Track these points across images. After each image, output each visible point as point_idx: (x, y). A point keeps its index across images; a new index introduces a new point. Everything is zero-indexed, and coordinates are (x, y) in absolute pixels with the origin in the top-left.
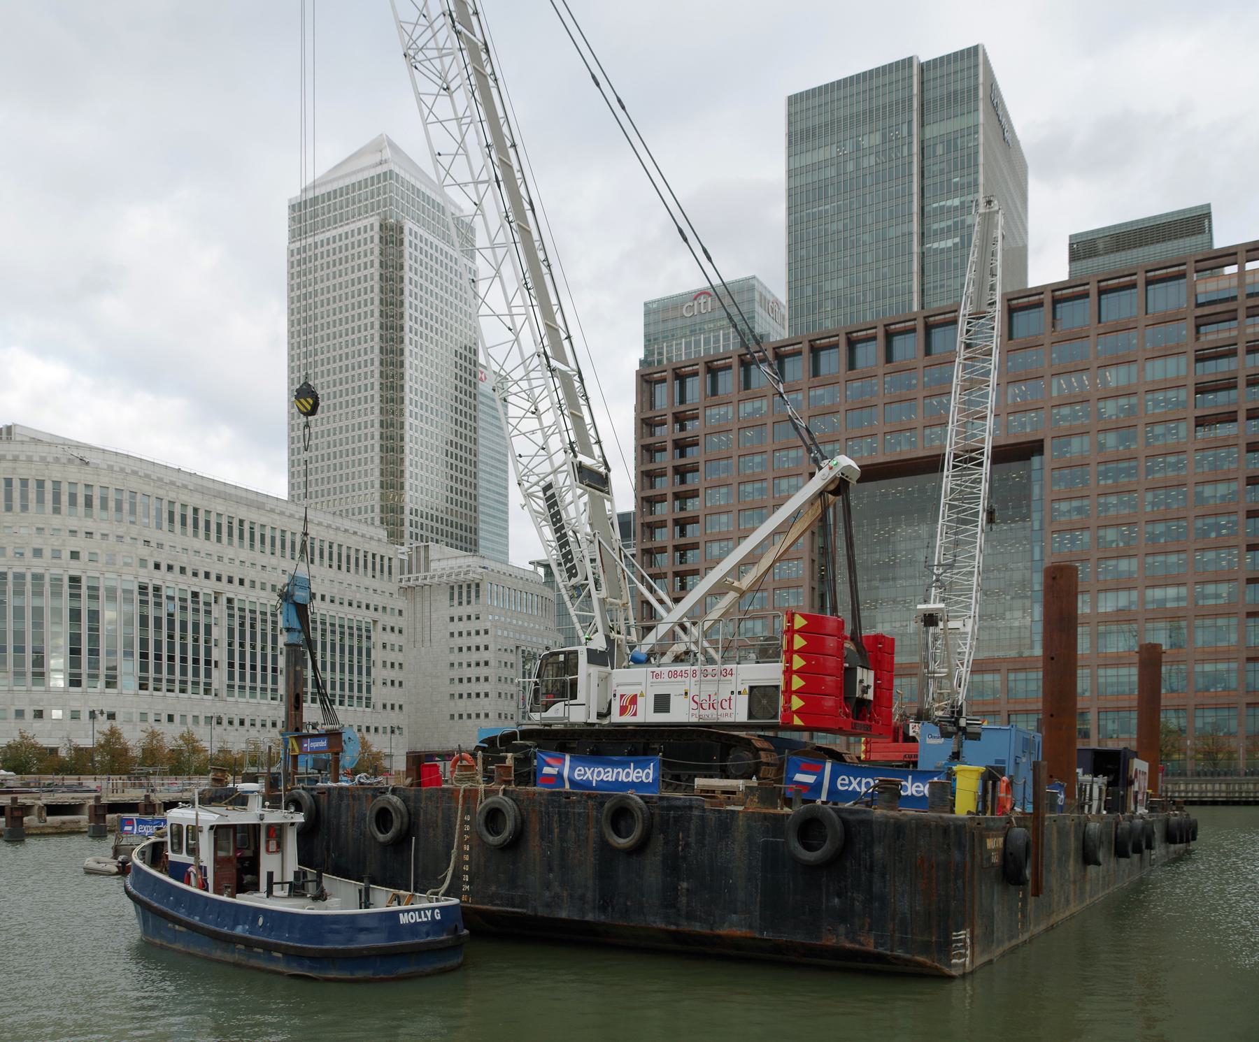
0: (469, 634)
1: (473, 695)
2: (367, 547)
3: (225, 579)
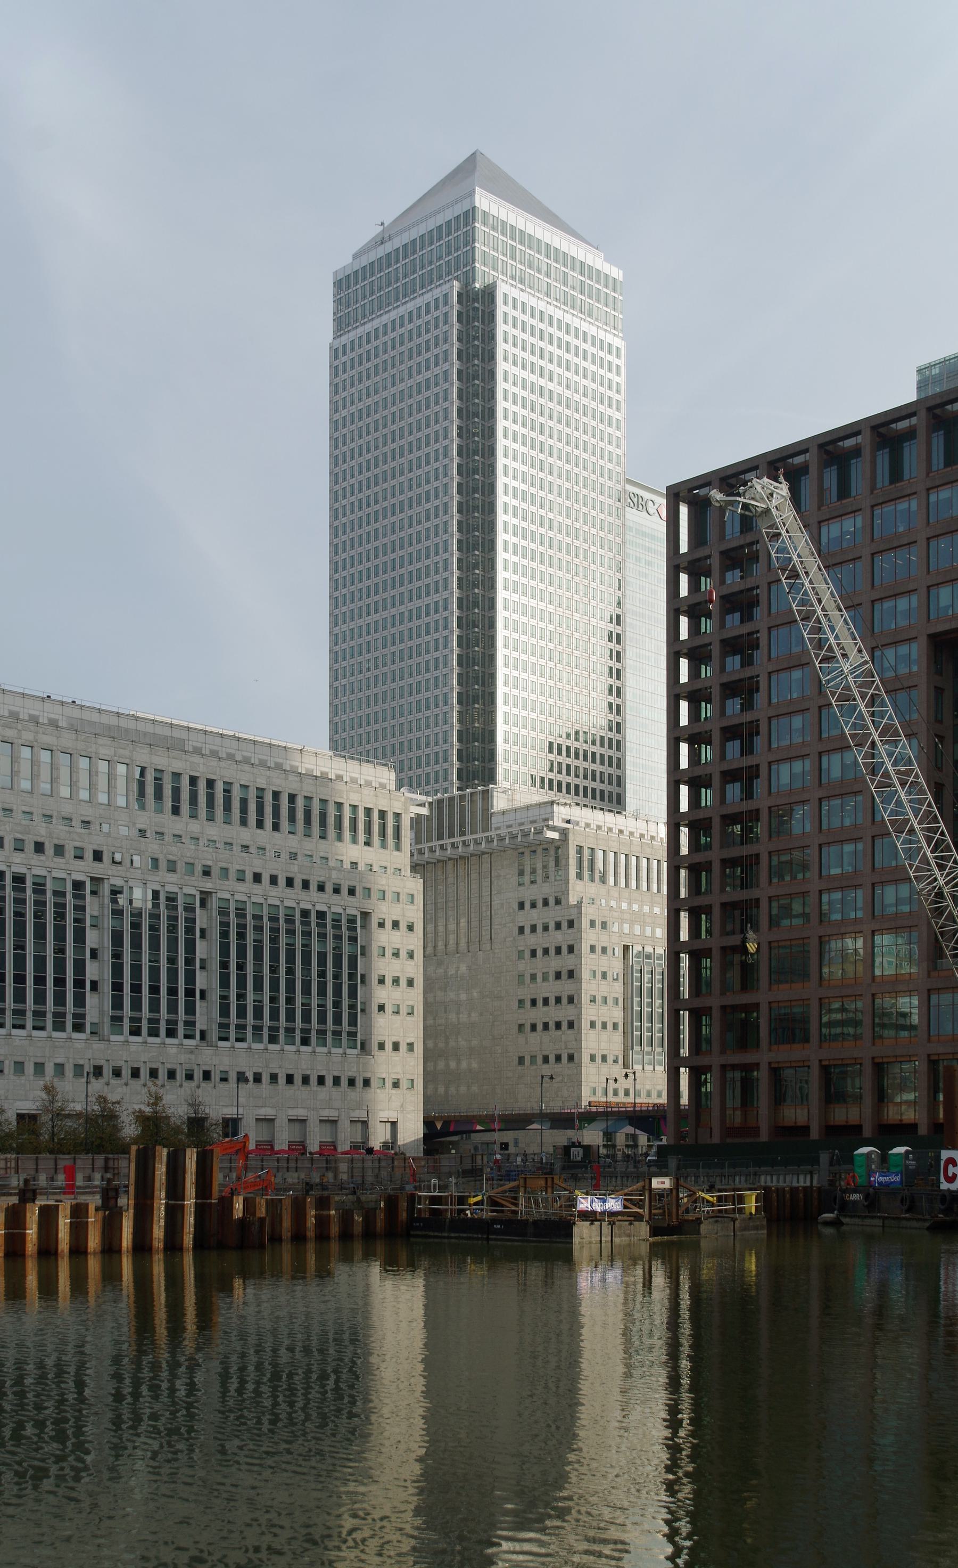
0: (546, 928)
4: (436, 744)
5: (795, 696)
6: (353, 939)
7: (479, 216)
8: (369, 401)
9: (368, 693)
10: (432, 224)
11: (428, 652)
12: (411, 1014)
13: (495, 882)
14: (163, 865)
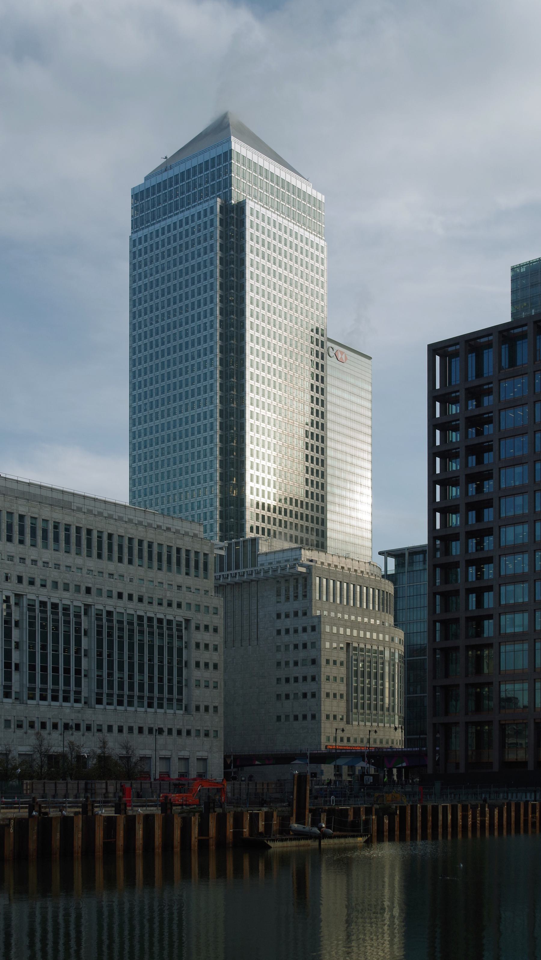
0: (296, 631)
2: (179, 543)
3: (25, 581)
4: (205, 507)
5: (517, 483)
6: (180, 637)
7: (234, 156)
8: (158, 276)
9: (157, 472)
10: (201, 160)
11: (199, 445)
12: (215, 687)
14: (61, 586)
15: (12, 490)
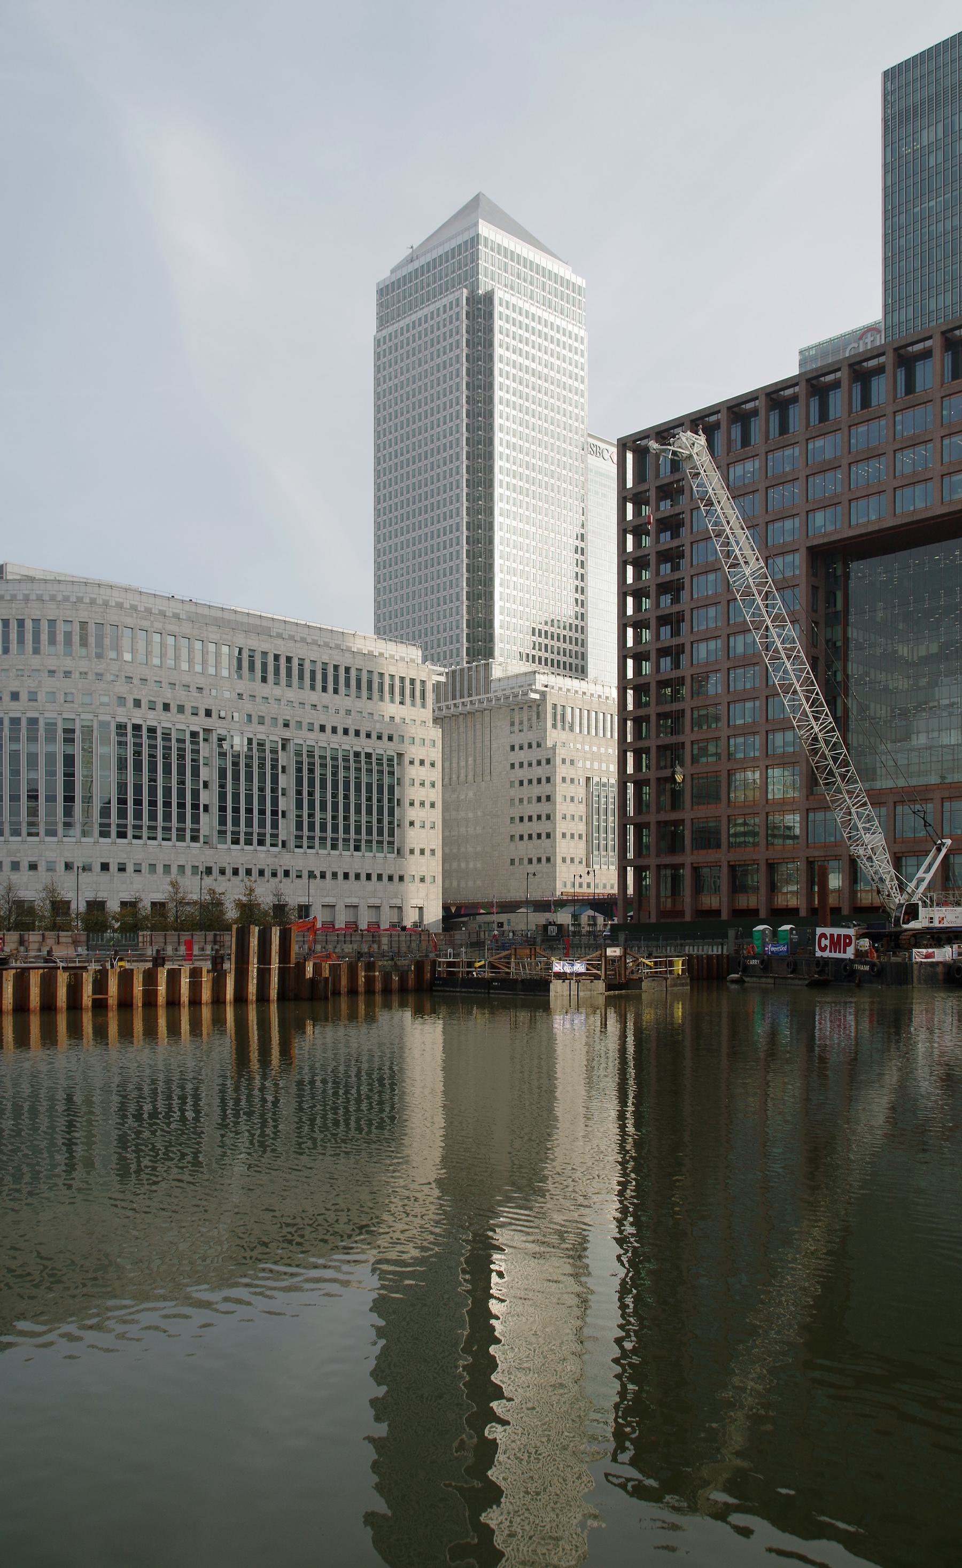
0: (530, 765)
1: (535, 836)
4: (451, 629)
6: (391, 773)
7: (482, 241)
10: (447, 247)
13: (493, 730)
14: (255, 719)
15: (204, 616)
